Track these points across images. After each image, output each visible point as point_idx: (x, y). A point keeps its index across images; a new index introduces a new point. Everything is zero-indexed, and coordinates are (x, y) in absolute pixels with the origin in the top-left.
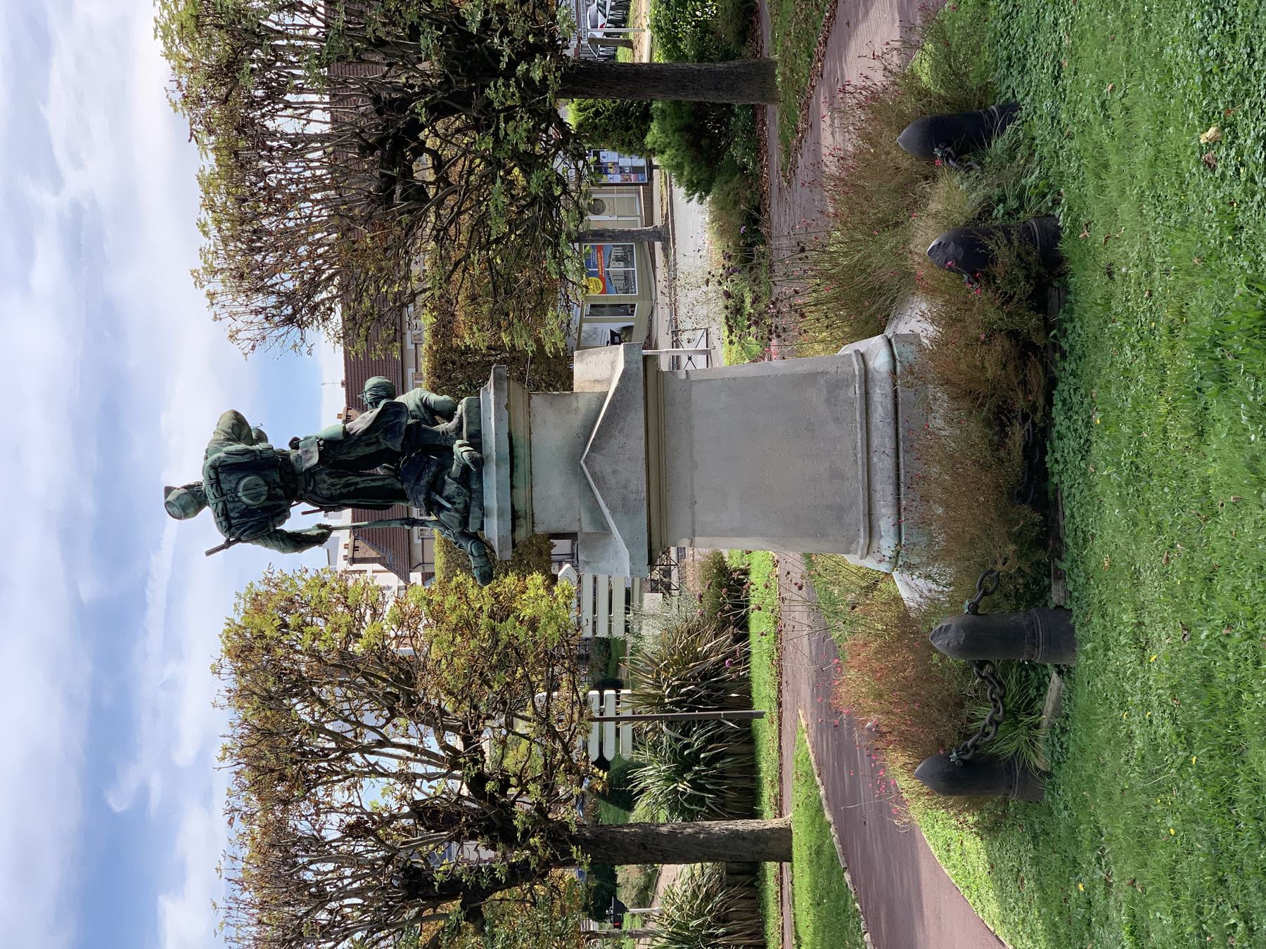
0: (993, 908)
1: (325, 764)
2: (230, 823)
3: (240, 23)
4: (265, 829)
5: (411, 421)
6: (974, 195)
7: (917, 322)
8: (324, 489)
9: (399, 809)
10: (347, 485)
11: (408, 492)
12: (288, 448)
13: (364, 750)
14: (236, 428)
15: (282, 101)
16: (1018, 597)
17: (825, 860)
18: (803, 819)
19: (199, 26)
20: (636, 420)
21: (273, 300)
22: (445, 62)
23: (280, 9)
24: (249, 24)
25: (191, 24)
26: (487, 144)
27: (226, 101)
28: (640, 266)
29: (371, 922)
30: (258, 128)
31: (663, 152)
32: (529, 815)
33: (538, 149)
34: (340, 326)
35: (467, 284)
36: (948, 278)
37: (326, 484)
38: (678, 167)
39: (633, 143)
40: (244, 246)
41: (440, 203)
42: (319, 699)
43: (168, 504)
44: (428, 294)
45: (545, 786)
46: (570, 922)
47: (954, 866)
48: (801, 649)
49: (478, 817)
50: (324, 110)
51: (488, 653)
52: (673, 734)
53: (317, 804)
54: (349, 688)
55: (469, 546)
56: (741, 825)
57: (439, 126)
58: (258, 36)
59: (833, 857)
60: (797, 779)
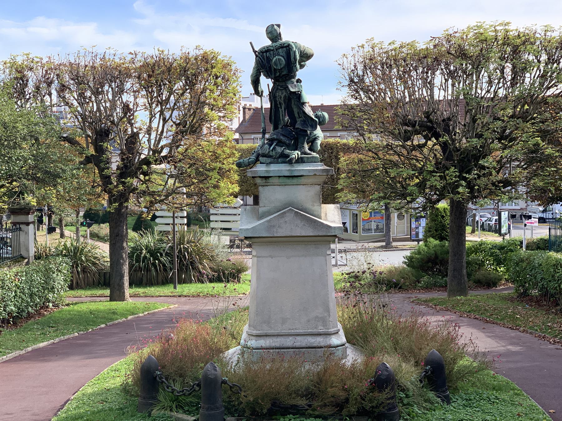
0: (90, 390)
1: (155, 95)
2: (131, 53)
3: (483, 59)
4: (127, 68)
5: (309, 132)
6: (409, 383)
7: (352, 357)
8: (279, 94)
9: (135, 127)
10: (280, 104)
11: (277, 131)
12: (297, 78)
13: (162, 112)
14: (306, 55)
15: (449, 78)
16: (230, 402)
17: (111, 316)
18: (129, 306)
19: (482, 41)
20: (309, 232)
21: (361, 73)
22: (466, 149)
23: (489, 77)
24: (483, 63)
25: (483, 38)
26: (430, 168)
27: (449, 53)
28: (374, 236)
29: (85, 115)
30: (437, 67)
31: (426, 246)
32: (132, 184)
33: (427, 191)
34: (349, 103)
35: (367, 158)
36: (372, 372)
37: (281, 95)
38: (419, 253)
39: (429, 232)
40: (384, 61)
41: (403, 146)
42: (184, 92)
43: (273, 25)
44: (363, 142)
45: (144, 192)
46: (84, 203)
47: (108, 373)
48: (210, 306)
49: (131, 161)
50: (445, 96)
51: (204, 167)
52: (167, 248)
53: (138, 91)
54: (189, 105)
55: (253, 157)
56: (126, 279)
57: (437, 147)
58: (477, 67)
59: (112, 320)
60: (147, 304)
